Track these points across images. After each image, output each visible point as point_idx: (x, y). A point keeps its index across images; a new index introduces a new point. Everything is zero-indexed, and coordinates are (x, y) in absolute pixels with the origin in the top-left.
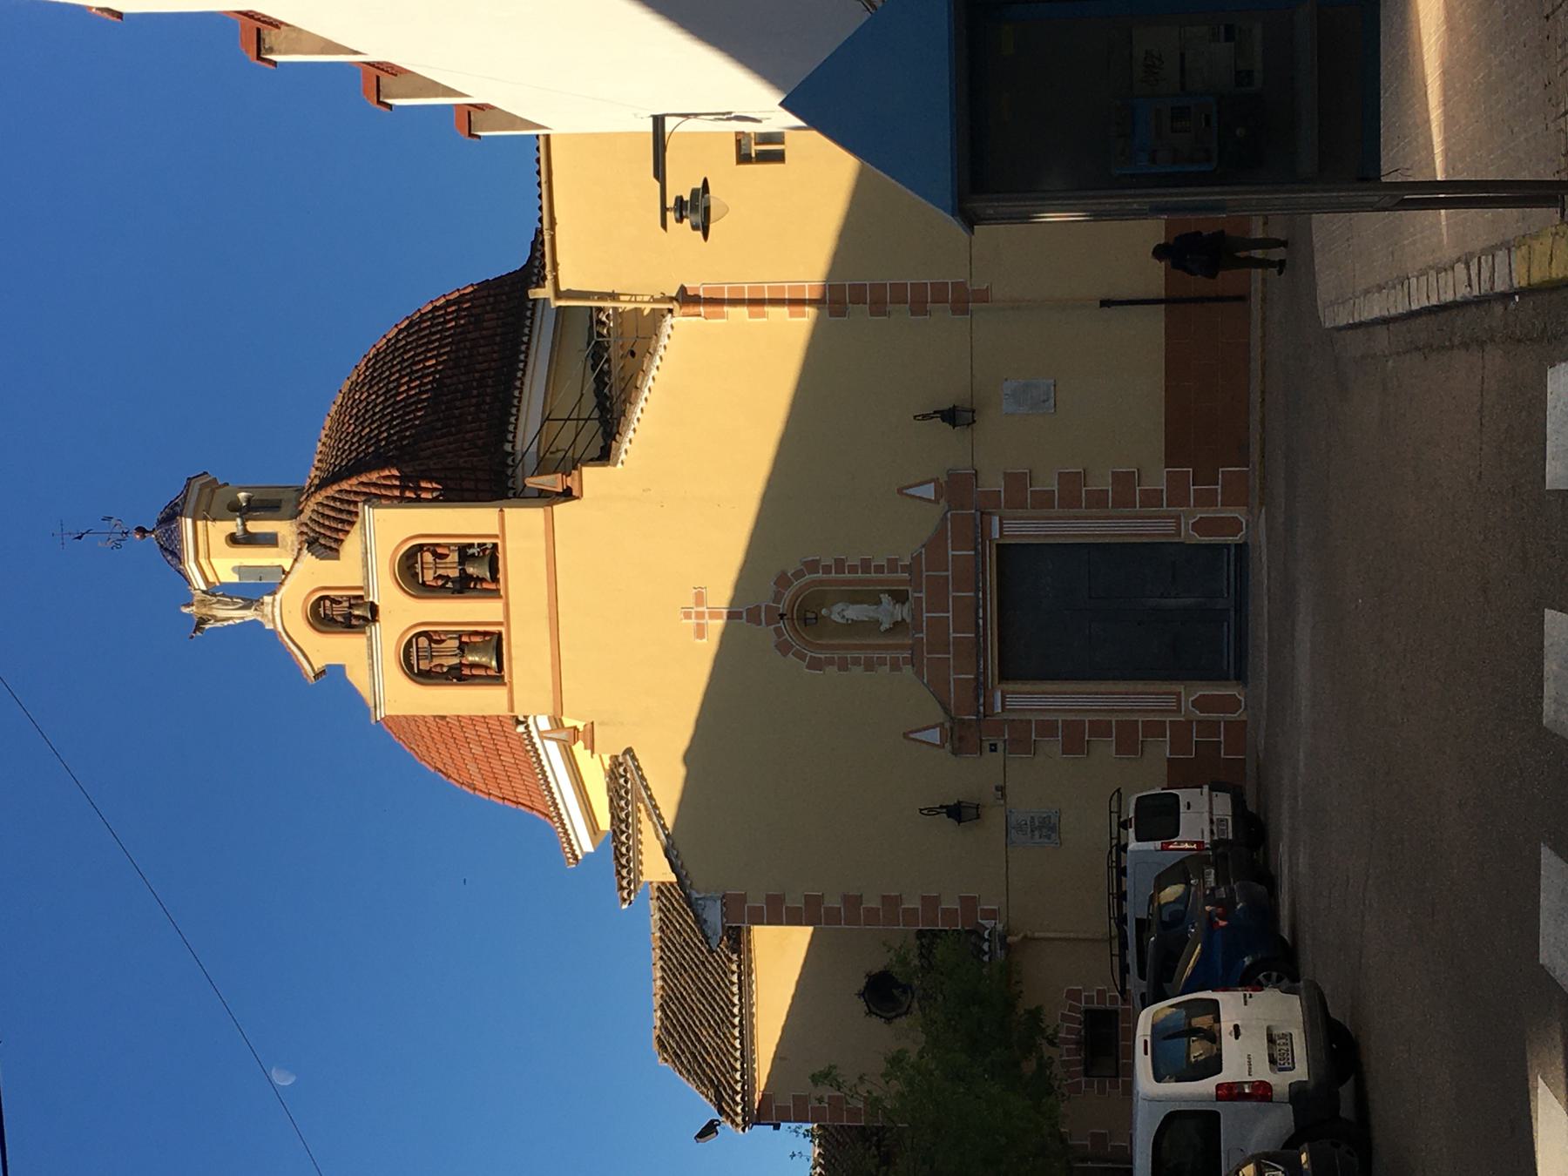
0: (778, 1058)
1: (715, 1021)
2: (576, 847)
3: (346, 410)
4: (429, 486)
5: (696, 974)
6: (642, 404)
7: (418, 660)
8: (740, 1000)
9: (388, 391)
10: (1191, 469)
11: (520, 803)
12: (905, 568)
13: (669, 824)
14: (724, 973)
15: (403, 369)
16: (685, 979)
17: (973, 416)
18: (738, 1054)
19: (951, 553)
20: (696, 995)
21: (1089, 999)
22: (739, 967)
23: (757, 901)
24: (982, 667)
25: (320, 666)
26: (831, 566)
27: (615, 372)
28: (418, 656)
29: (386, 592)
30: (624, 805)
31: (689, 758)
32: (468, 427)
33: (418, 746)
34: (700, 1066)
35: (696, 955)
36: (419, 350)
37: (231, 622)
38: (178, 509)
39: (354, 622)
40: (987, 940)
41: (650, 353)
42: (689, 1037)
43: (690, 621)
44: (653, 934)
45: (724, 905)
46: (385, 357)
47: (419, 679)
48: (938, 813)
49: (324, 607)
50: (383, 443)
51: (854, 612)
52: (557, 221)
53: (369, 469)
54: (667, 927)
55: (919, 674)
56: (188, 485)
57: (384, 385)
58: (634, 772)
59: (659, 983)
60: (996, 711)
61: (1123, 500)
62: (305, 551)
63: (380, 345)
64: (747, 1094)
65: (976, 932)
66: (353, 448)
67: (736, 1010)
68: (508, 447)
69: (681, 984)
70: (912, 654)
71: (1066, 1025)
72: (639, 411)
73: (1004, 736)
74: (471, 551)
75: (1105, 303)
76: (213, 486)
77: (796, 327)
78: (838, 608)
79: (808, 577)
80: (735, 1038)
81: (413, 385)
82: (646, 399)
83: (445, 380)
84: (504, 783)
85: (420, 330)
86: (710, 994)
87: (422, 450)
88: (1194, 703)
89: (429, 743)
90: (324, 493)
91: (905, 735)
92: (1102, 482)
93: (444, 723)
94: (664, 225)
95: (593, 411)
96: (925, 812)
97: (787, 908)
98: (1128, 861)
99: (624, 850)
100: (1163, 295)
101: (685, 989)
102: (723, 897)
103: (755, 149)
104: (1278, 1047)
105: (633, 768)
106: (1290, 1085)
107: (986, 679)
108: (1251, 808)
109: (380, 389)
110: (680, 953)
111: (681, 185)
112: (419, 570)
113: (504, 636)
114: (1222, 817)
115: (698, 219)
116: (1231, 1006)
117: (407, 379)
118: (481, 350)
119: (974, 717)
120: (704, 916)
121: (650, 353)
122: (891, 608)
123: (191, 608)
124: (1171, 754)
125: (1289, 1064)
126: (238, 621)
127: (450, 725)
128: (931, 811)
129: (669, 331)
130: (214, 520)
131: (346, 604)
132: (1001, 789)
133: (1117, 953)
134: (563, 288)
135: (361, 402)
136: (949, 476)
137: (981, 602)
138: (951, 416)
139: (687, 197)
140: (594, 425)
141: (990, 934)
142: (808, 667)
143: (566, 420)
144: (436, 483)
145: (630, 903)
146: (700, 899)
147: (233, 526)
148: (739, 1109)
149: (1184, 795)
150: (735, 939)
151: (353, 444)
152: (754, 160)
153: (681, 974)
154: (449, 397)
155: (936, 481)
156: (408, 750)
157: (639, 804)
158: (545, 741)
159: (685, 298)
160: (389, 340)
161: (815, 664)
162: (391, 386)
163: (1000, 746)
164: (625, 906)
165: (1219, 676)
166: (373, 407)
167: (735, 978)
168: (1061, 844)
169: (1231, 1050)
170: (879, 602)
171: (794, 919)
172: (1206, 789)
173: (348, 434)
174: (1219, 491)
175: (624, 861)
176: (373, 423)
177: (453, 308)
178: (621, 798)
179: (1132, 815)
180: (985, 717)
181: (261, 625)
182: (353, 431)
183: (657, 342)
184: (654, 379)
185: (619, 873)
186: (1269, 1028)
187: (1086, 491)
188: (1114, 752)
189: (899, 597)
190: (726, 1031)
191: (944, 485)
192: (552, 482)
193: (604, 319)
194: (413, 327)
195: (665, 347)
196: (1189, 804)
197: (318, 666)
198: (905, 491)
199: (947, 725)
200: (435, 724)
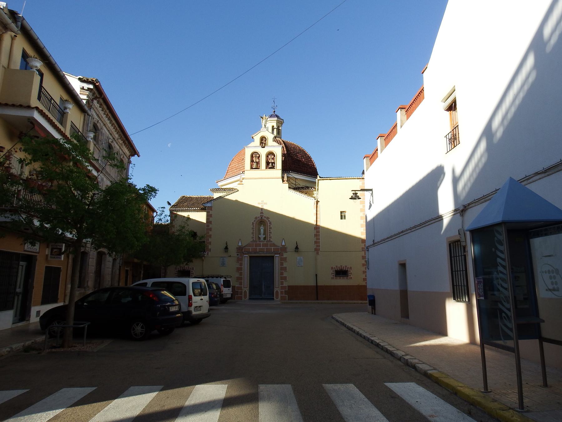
2: (219, 182)
18: (183, 209)
19: (273, 248)
21: (192, 271)
23: (211, 212)
31: (236, 201)
34: (180, 203)
37: (262, 123)
39: (262, 144)
51: (262, 231)
55: (251, 242)
59: (194, 197)
61: (282, 278)
64: (176, 210)
65: (204, 251)
67: (191, 209)
68: (291, 172)
75: (316, 275)
76: (282, 124)
77: (312, 221)
79: (268, 223)
85: (309, 158)
88: (245, 291)
89: (238, 158)
92: (285, 274)
94: (352, 191)
98: (219, 279)
99: (220, 190)
100: (318, 285)
103: (343, 214)
107: (250, 254)
108: (228, 301)
111: (359, 194)
115: (354, 196)
116: (206, 298)
138: (297, 248)
139: (357, 195)
140: (294, 186)
147: (275, 127)
148: (173, 209)
149: (231, 289)
155: (285, 245)
159: (317, 202)
161: (253, 223)
163: (238, 256)
165: (250, 294)
167: (196, 209)
171: (207, 219)
172: (232, 293)
175: (218, 190)
178: (229, 190)
179: (227, 279)
186: (202, 306)
189: (265, 238)
192: (286, 179)
197: (254, 137)
199: (242, 247)
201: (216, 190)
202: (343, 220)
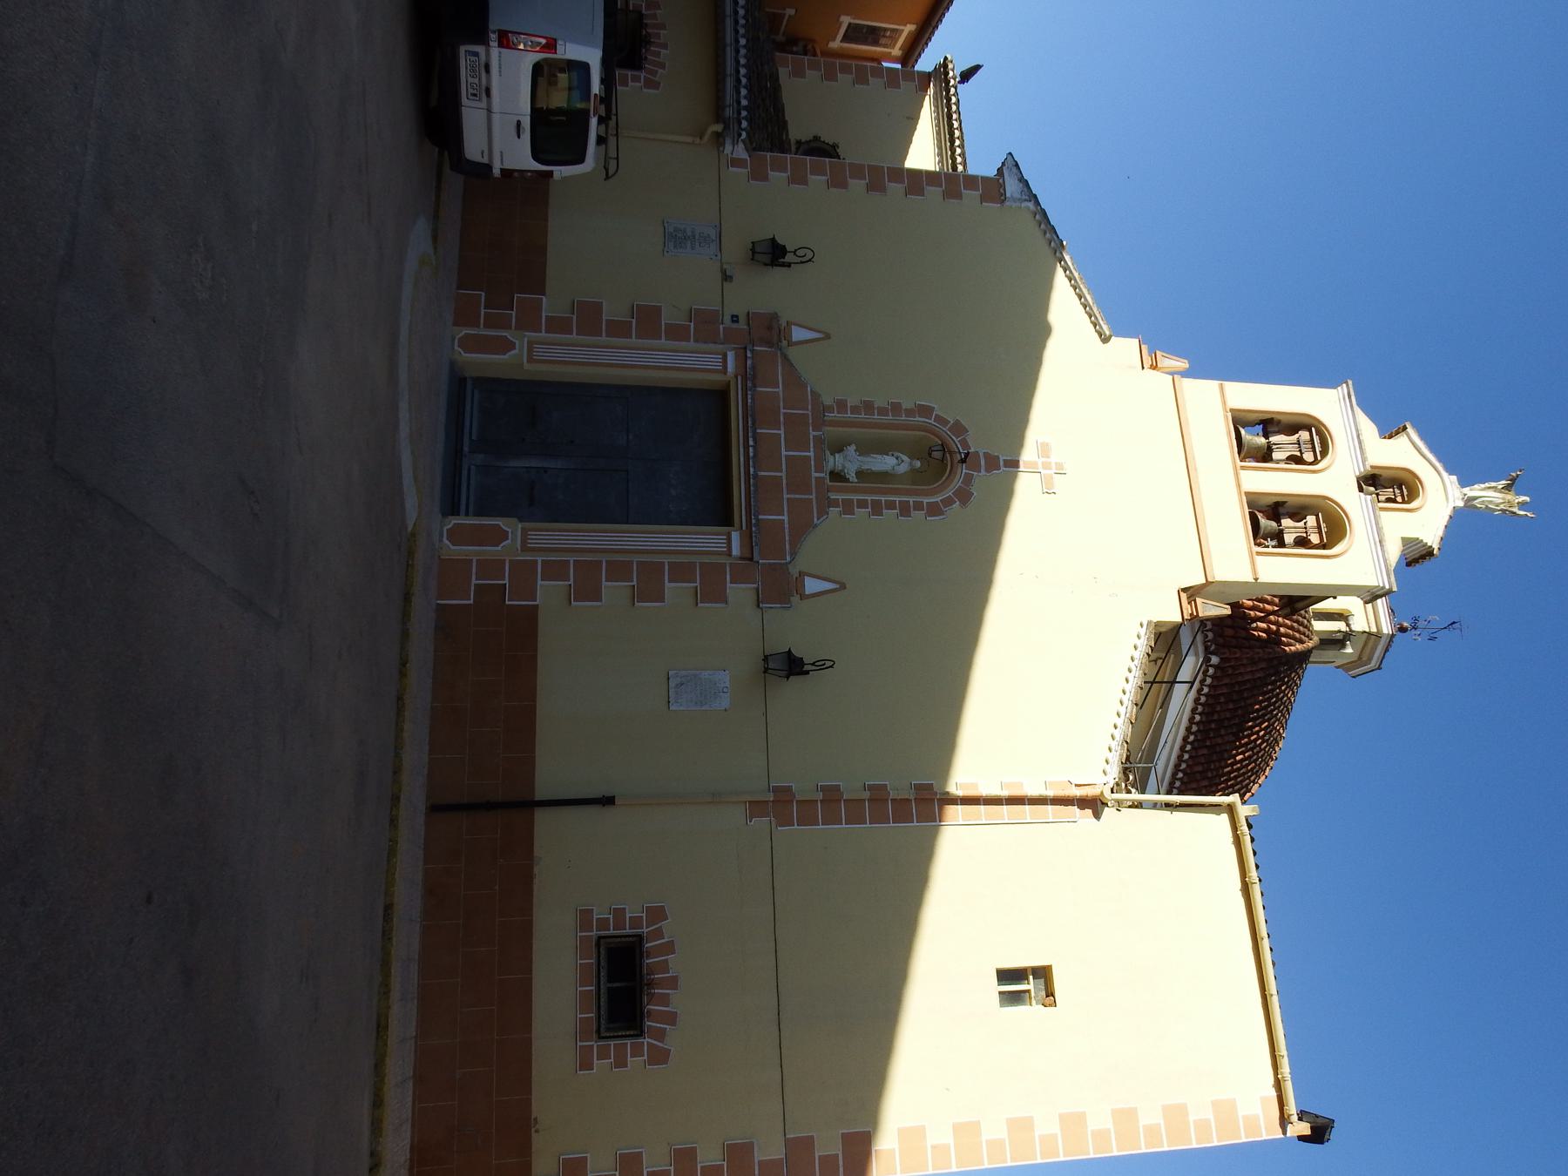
0: (913, 119)
6: (1128, 687)
10: (507, 602)
12: (835, 503)
24: (749, 396)
26: (915, 509)
29: (1355, 505)
31: (1045, 330)
37: (1483, 486)
47: (1312, 421)
51: (885, 463)
52: (1240, 893)
55: (816, 396)
60: (733, 352)
65: (753, 147)
72: (1131, 679)
73: (724, 328)
75: (608, 801)
77: (960, 780)
78: (903, 468)
88: (512, 346)
92: (612, 590)
102: (1003, 201)
103: (1030, 985)
121: (1126, 742)
122: (848, 465)
123: (1520, 500)
124: (542, 299)
129: (1108, 768)
136: (789, 602)
138: (793, 666)
141: (740, 135)
146: (1026, 200)
152: (1029, 972)
155: (803, 597)
159: (1094, 805)
161: (925, 411)
163: (727, 319)
165: (492, 386)
170: (860, 474)
172: (496, 172)
174: (474, 577)
180: (745, 348)
187: (632, 581)
188: (604, 304)
189: (837, 476)
199: (785, 343)
202: (994, 988)
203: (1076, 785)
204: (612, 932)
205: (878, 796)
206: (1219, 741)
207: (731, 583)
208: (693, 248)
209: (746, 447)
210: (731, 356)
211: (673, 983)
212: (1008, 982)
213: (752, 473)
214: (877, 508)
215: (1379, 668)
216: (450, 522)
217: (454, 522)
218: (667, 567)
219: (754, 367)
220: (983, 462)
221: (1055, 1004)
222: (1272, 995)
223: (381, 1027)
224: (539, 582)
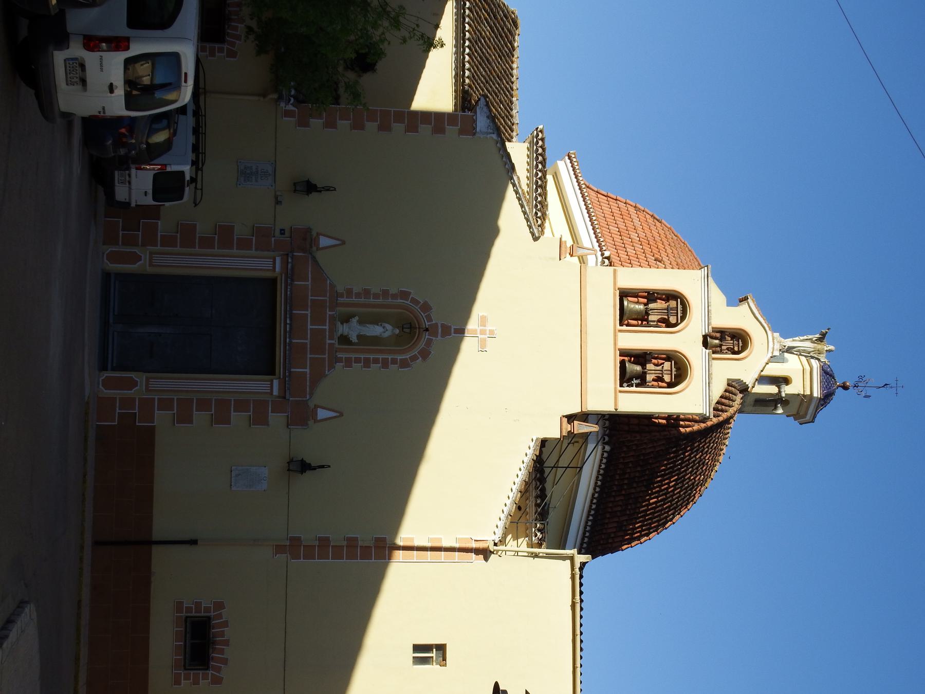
0: (439, 14)
1: (481, 42)
3: (710, 468)
4: (661, 421)
5: (492, 74)
6: (518, 481)
7: (677, 308)
8: (464, 58)
9: (682, 482)
10: (137, 424)
11: (606, 196)
12: (339, 360)
13: (510, 187)
14: (474, 77)
15: (672, 496)
16: (499, 69)
17: (289, 466)
18: (467, 20)
19: (308, 370)
20: (492, 59)
22: (464, 81)
25: (744, 306)
26: (391, 364)
27: (532, 499)
28: (677, 311)
29: (695, 354)
30: (539, 197)
32: (632, 459)
33: (672, 239)
34: (492, 10)
35: (491, 87)
36: (660, 508)
37: (802, 338)
38: (822, 403)
39: (718, 335)
40: (291, 96)
41: (511, 516)
42: (498, 30)
43: (490, 328)
44: (517, 100)
45: (475, 128)
46: (682, 503)
48: (323, 188)
49: (739, 346)
50: (688, 449)
51: (375, 330)
53: (699, 432)
54: (508, 105)
55: (332, 286)
56: (814, 417)
57: (685, 485)
58: (533, 224)
59: (515, 66)
60: (280, 257)
62: (750, 386)
63: (685, 511)
65: (299, 101)
66: (708, 445)
67: (467, 50)
68: (607, 448)
69: (501, 66)
70: (337, 300)
71: (238, 33)
72: (519, 476)
74: (638, 381)
75: (194, 542)
77: (405, 535)
79: (407, 356)
80: (468, 31)
81: (666, 486)
82: (514, 483)
83: (645, 489)
84: (616, 210)
86: (483, 60)
87: (663, 444)
89: (665, 240)
90: (728, 414)
91: (344, 243)
92: (200, 418)
93: (656, 256)
95: (548, 476)
96: (332, 189)
97: (431, 124)
98: (191, 156)
101: (499, 63)
102: (474, 134)
103: (433, 654)
104: (78, 76)
105: (534, 227)
106: (68, 48)
108: (101, 190)
109: (688, 483)
110: (501, 87)
112: (674, 369)
113: (618, 322)
114: (121, 185)
116: (116, 106)
117: (670, 490)
118: (619, 508)
119: (295, 254)
120: (488, 121)
121: (511, 516)
123: (828, 349)
124: (158, 222)
125: (69, 64)
126: (797, 338)
127: (652, 254)
128: (328, 189)
129: (496, 530)
130: (798, 395)
131: (724, 347)
132: (278, 202)
133: (200, 90)
134: (568, 562)
135: (700, 474)
136: (307, 425)
137: (288, 336)
138: (304, 467)
140: (550, 463)
141: (290, 100)
142: (410, 293)
143: (568, 467)
144: (655, 422)
145: (537, 129)
146: (491, 133)
147: (787, 390)
149: (149, 201)
150: (466, 101)
151: (708, 447)
153: (501, 73)
154: (643, 479)
155: (316, 421)
156: (679, 235)
157: (528, 197)
158: (591, 247)
159: (485, 553)
160: (679, 514)
161: (405, 295)
162: (680, 485)
163: (277, 233)
164: (541, 127)
165: (124, 278)
166: (689, 465)
167: (467, 73)
168: (237, 162)
169: (117, 75)
170: (359, 337)
171: (426, 116)
172: (133, 205)
173: (710, 453)
174: (117, 409)
175: (540, 158)
176: (694, 461)
177: (636, 535)
178: (540, 202)
179: (187, 189)
180: (288, 255)
181: (781, 336)
182: (707, 455)
183: (505, 523)
184: (509, 498)
185: (544, 150)
189: (344, 340)
190: (474, 36)
191: (311, 418)
192: (580, 428)
193: (539, 534)
194: (663, 523)
195: (500, 519)
196: (146, 195)
197: (744, 307)
198: (338, 414)
199: (314, 248)
200: (662, 255)
201: (540, 150)
202: (410, 654)
203: (475, 540)
204: (193, 614)
205: (352, 543)
206: (633, 491)
207: (271, 413)
208: (256, 181)
209: (286, 324)
210: (278, 260)
211: (227, 643)
212: (418, 652)
213: (288, 342)
214: (367, 363)
215: (813, 422)
216: (104, 375)
217: (106, 375)
218: (233, 403)
219: (293, 268)
220: (440, 331)
221: (445, 665)
222: (577, 667)
223: (77, 659)
224: (156, 412)
